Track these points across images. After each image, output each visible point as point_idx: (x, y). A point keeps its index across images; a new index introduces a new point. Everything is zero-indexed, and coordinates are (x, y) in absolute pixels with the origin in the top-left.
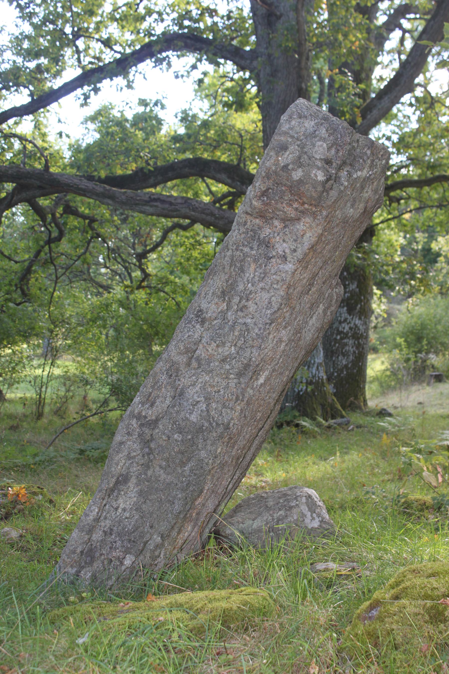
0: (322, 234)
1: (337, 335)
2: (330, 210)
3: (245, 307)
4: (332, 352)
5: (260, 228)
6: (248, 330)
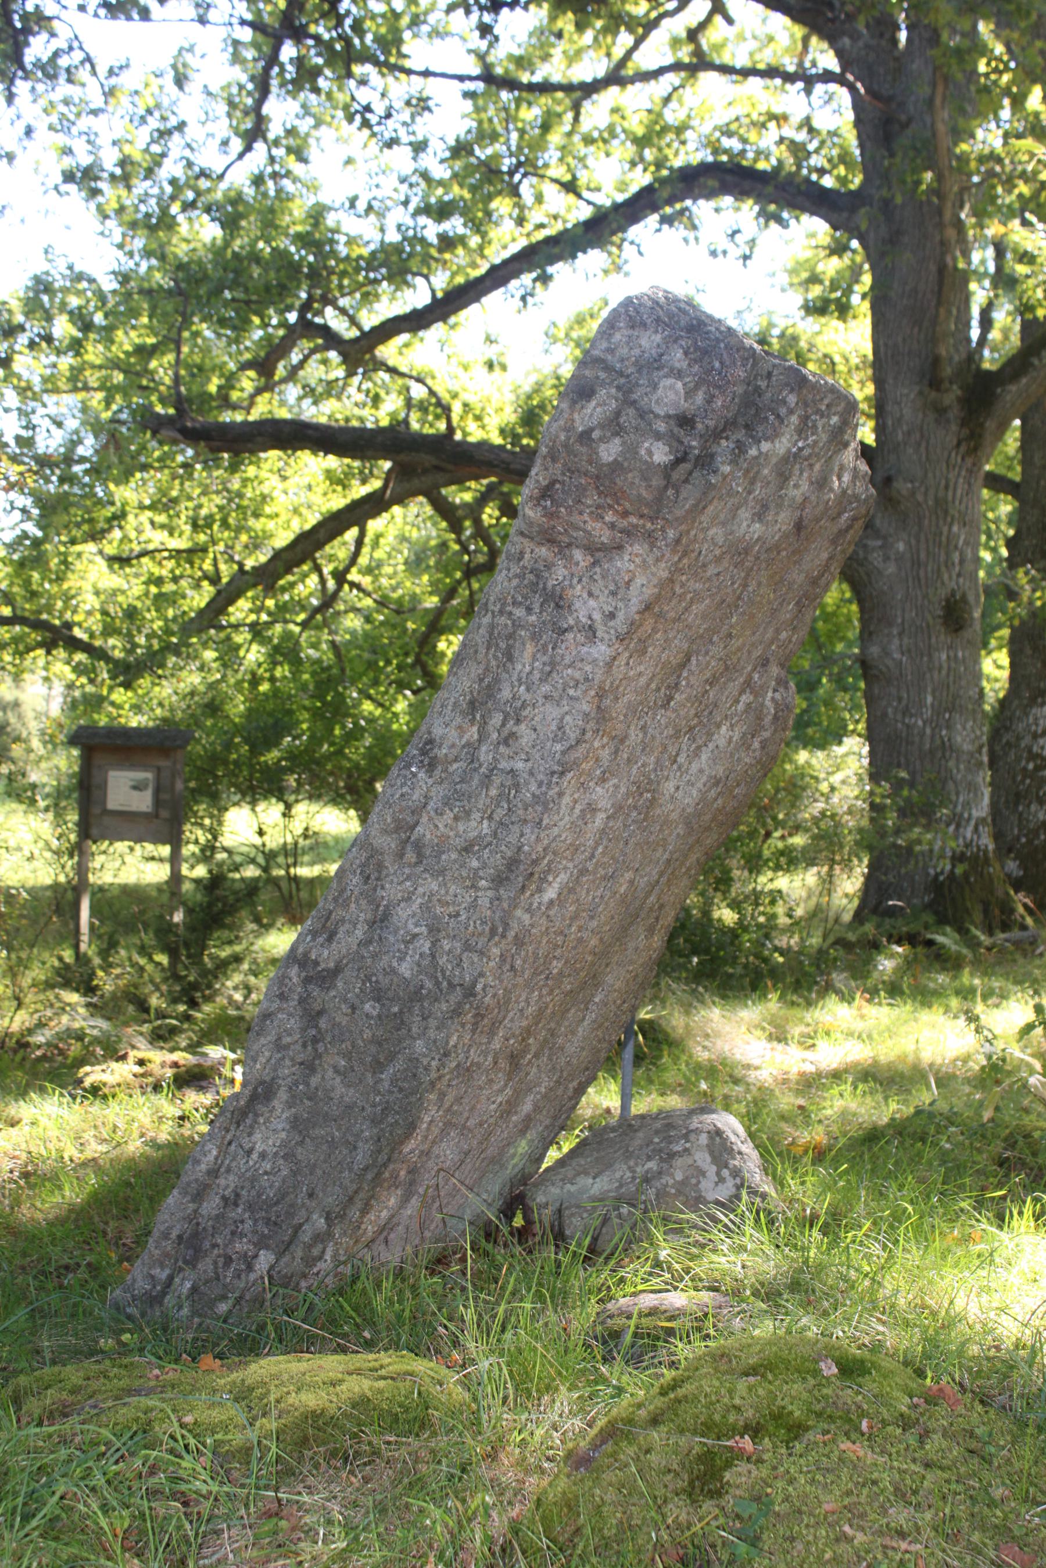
0: (671, 581)
1: (1028, 761)
2: (683, 527)
3: (512, 735)
4: (1018, 795)
5: (548, 567)
6: (517, 786)
